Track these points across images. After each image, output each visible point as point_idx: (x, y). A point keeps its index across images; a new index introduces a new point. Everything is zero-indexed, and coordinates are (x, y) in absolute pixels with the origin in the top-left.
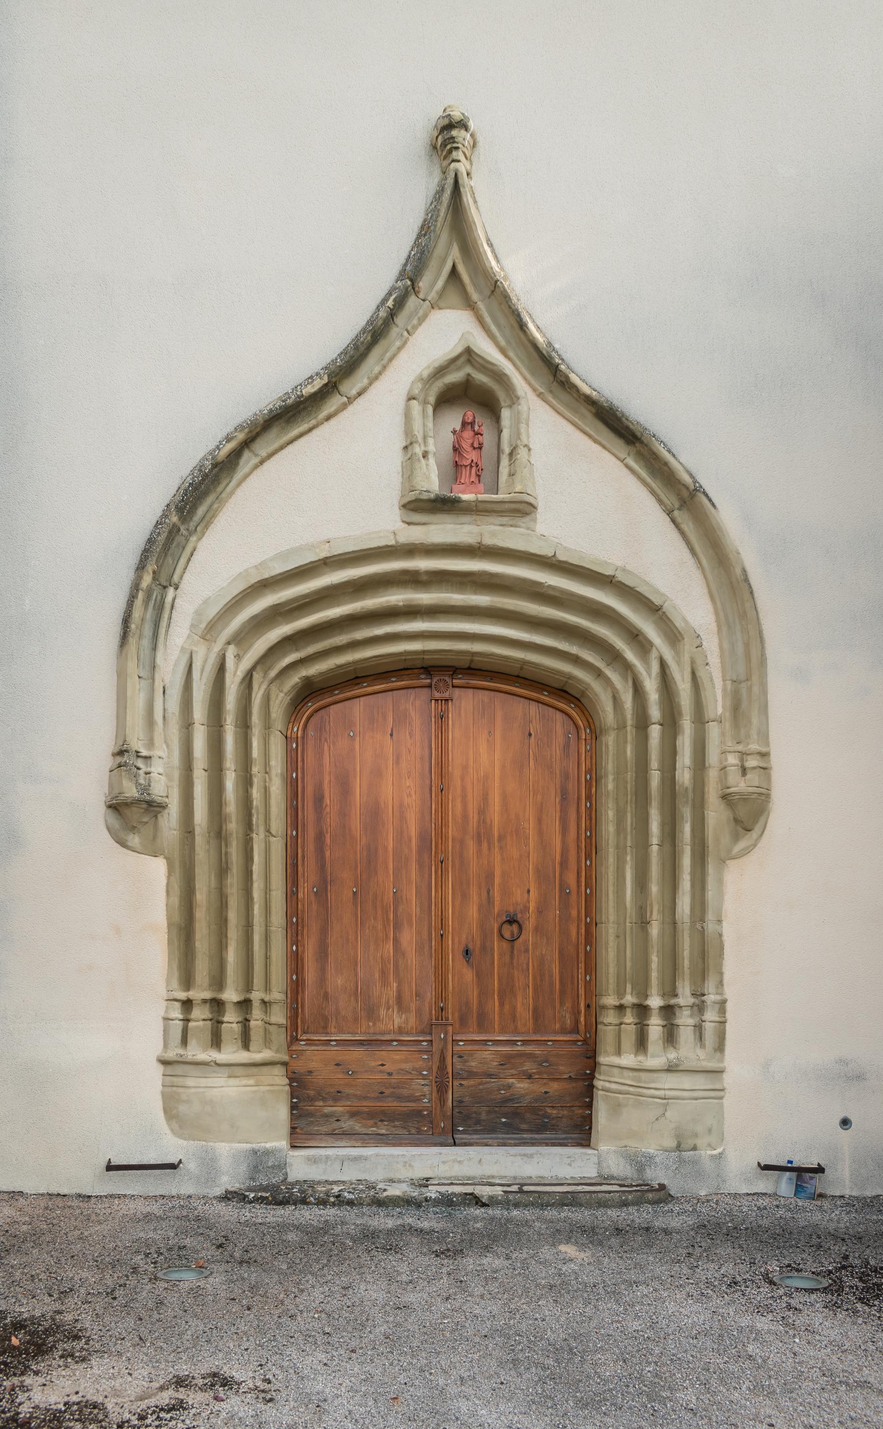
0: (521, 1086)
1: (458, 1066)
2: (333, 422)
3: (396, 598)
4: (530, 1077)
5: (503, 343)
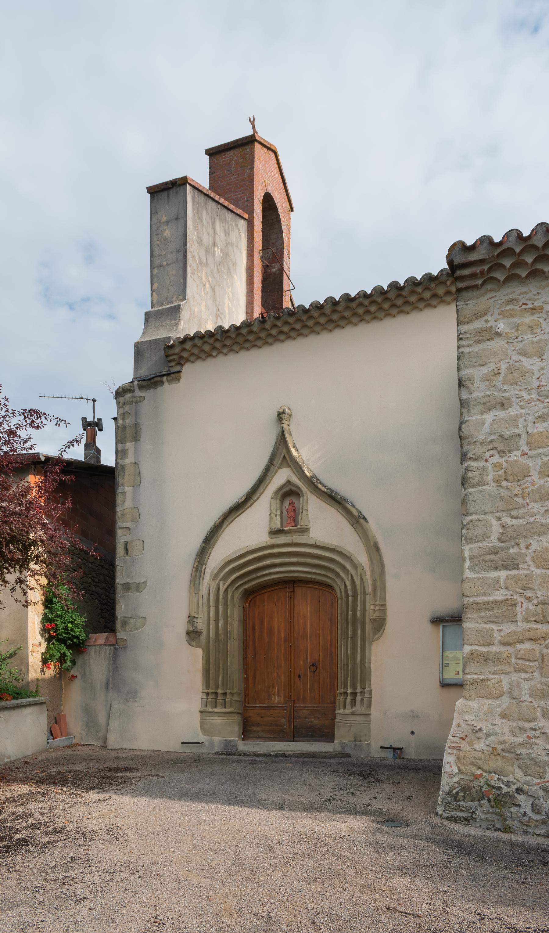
0: (316, 722)
1: (296, 714)
2: (250, 508)
3: (268, 562)
4: (319, 718)
5: (299, 477)
